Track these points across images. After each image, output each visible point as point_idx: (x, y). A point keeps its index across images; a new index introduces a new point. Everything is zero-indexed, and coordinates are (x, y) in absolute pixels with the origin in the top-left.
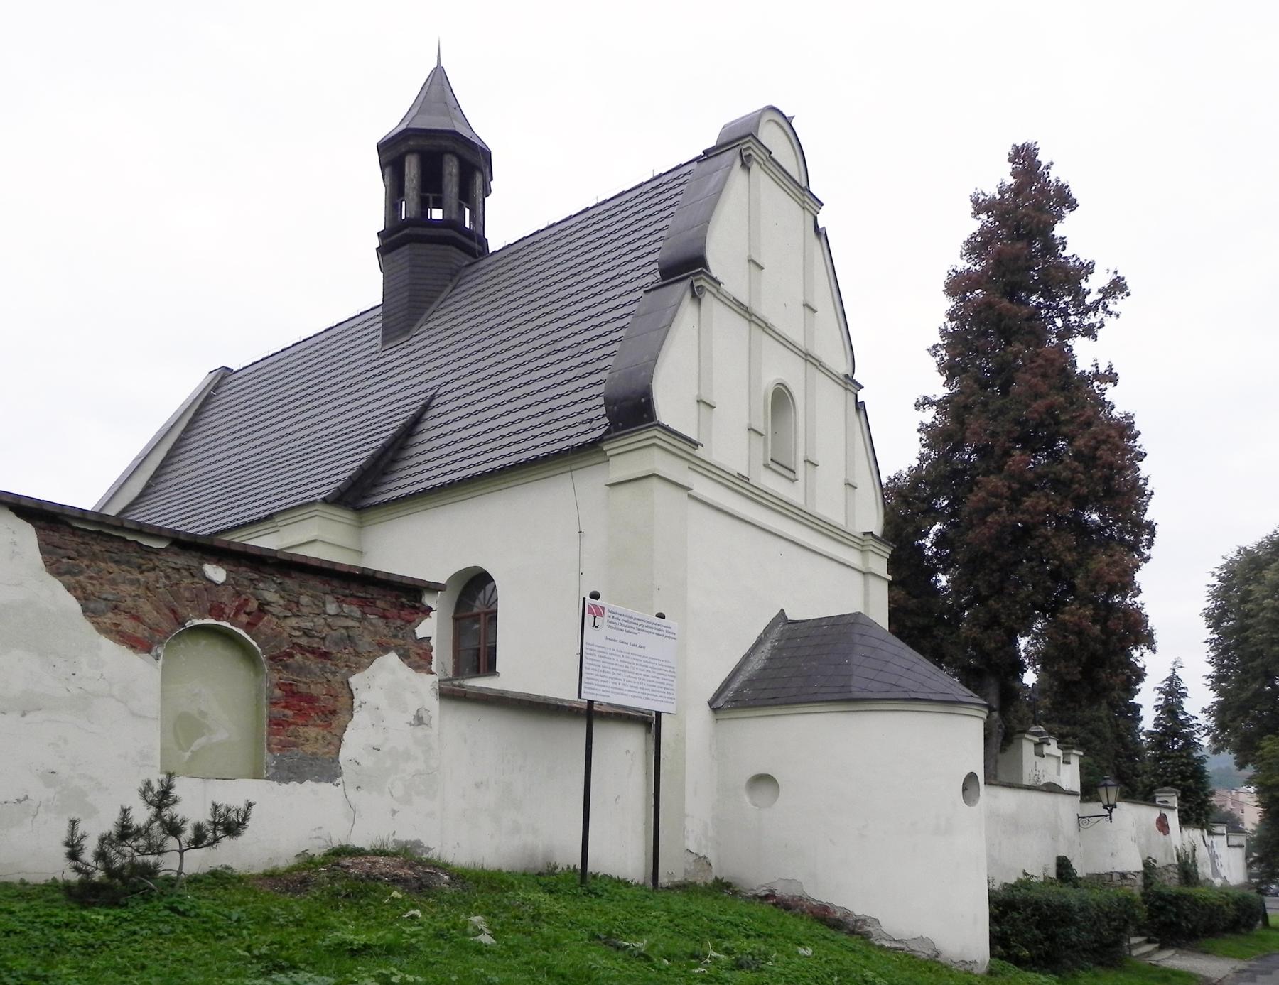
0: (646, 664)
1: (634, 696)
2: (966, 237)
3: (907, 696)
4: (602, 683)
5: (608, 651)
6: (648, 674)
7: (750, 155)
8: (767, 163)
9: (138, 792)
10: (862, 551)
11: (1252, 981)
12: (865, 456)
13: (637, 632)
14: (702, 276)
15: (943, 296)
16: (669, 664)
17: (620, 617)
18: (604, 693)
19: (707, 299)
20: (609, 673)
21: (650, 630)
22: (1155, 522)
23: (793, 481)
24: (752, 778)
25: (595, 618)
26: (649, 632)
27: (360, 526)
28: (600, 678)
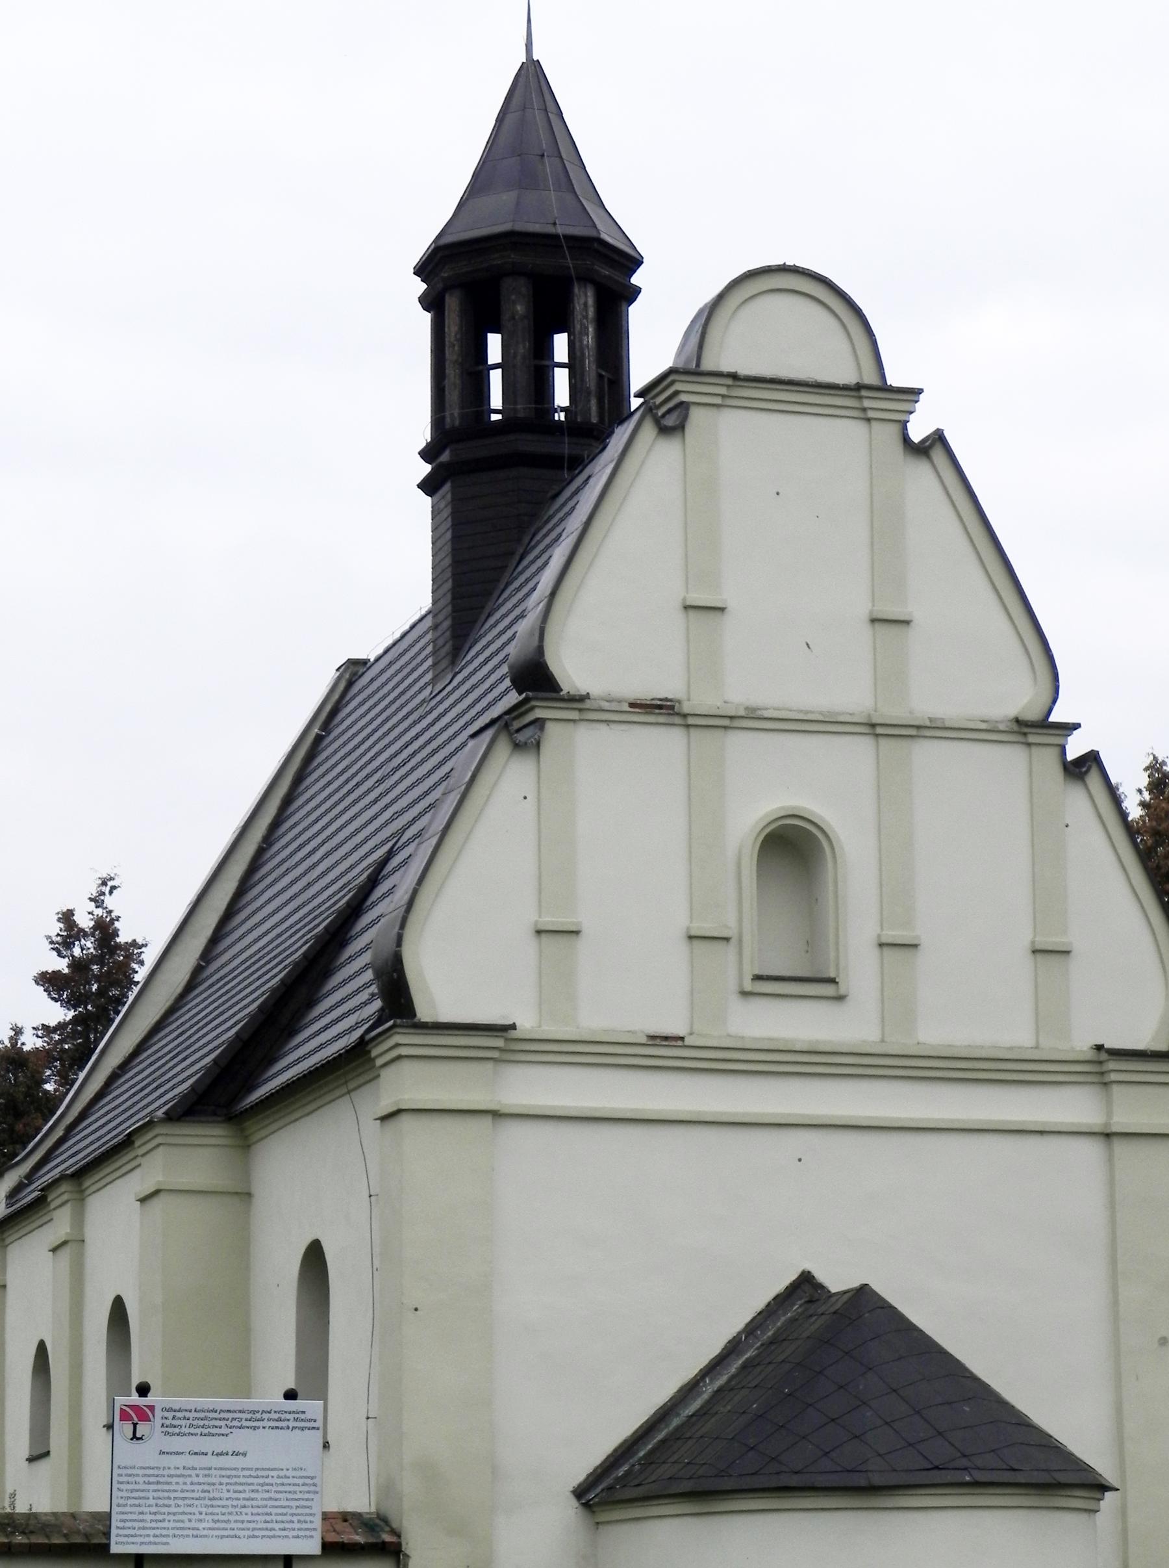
0: (250, 1480)
1: (222, 1537)
4: (154, 1525)
5: (166, 1472)
6: (253, 1495)
11: (325, 1512)
12: (1116, 864)
14: (534, 703)
17: (187, 1414)
18: (157, 1540)
20: (169, 1506)
23: (840, 998)
25: (135, 1425)
27: (245, 1145)
28: (149, 1517)
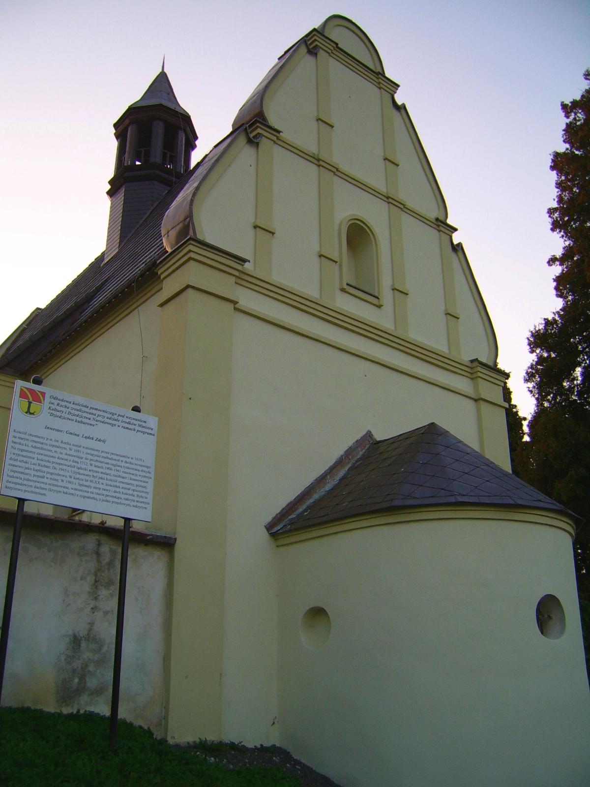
2: (554, 287)
3: (453, 500)
4: (35, 479)
6: (108, 471)
7: (317, 45)
8: (335, 52)
9: (101, 521)
10: (472, 379)
13: (94, 422)
15: (552, 172)
16: (142, 463)
19: (264, 143)
21: (114, 422)
22: (532, 329)
23: (379, 306)
24: (312, 608)
25: (30, 403)
26: (113, 425)
